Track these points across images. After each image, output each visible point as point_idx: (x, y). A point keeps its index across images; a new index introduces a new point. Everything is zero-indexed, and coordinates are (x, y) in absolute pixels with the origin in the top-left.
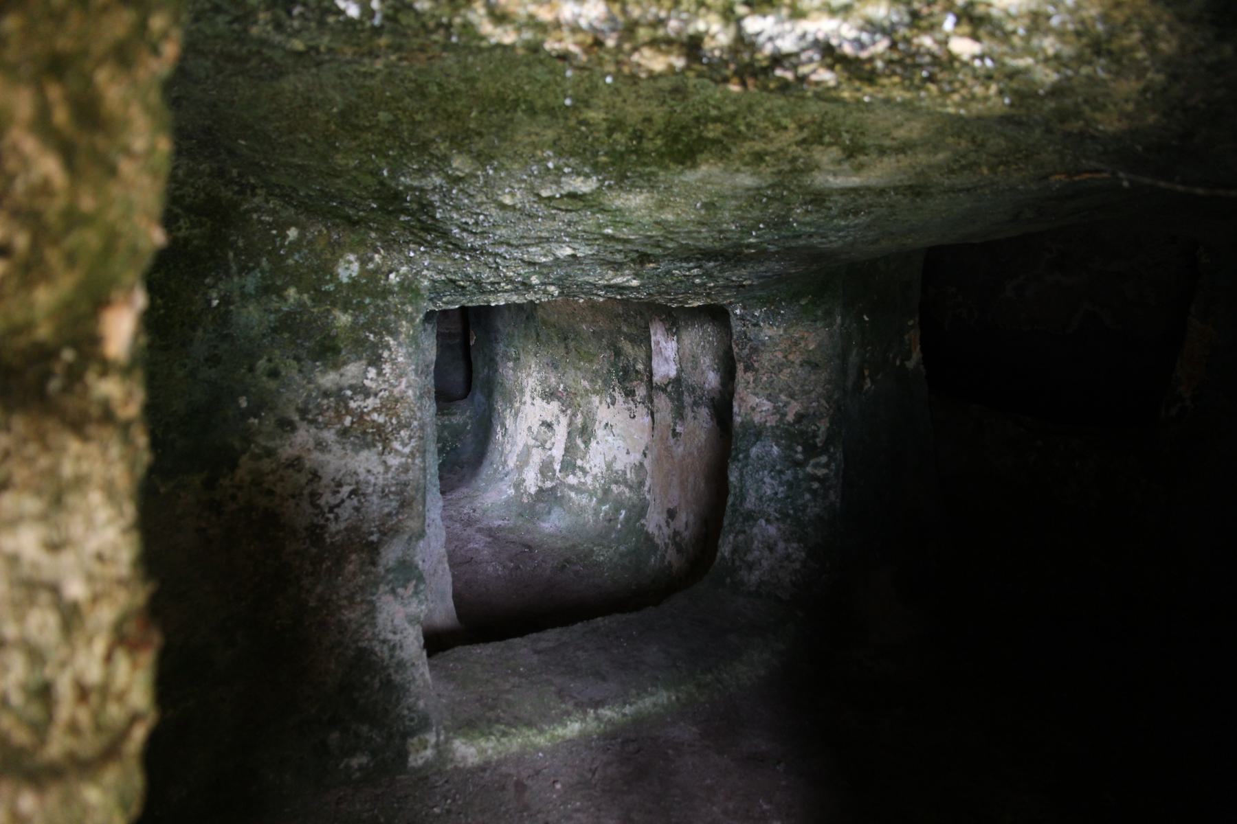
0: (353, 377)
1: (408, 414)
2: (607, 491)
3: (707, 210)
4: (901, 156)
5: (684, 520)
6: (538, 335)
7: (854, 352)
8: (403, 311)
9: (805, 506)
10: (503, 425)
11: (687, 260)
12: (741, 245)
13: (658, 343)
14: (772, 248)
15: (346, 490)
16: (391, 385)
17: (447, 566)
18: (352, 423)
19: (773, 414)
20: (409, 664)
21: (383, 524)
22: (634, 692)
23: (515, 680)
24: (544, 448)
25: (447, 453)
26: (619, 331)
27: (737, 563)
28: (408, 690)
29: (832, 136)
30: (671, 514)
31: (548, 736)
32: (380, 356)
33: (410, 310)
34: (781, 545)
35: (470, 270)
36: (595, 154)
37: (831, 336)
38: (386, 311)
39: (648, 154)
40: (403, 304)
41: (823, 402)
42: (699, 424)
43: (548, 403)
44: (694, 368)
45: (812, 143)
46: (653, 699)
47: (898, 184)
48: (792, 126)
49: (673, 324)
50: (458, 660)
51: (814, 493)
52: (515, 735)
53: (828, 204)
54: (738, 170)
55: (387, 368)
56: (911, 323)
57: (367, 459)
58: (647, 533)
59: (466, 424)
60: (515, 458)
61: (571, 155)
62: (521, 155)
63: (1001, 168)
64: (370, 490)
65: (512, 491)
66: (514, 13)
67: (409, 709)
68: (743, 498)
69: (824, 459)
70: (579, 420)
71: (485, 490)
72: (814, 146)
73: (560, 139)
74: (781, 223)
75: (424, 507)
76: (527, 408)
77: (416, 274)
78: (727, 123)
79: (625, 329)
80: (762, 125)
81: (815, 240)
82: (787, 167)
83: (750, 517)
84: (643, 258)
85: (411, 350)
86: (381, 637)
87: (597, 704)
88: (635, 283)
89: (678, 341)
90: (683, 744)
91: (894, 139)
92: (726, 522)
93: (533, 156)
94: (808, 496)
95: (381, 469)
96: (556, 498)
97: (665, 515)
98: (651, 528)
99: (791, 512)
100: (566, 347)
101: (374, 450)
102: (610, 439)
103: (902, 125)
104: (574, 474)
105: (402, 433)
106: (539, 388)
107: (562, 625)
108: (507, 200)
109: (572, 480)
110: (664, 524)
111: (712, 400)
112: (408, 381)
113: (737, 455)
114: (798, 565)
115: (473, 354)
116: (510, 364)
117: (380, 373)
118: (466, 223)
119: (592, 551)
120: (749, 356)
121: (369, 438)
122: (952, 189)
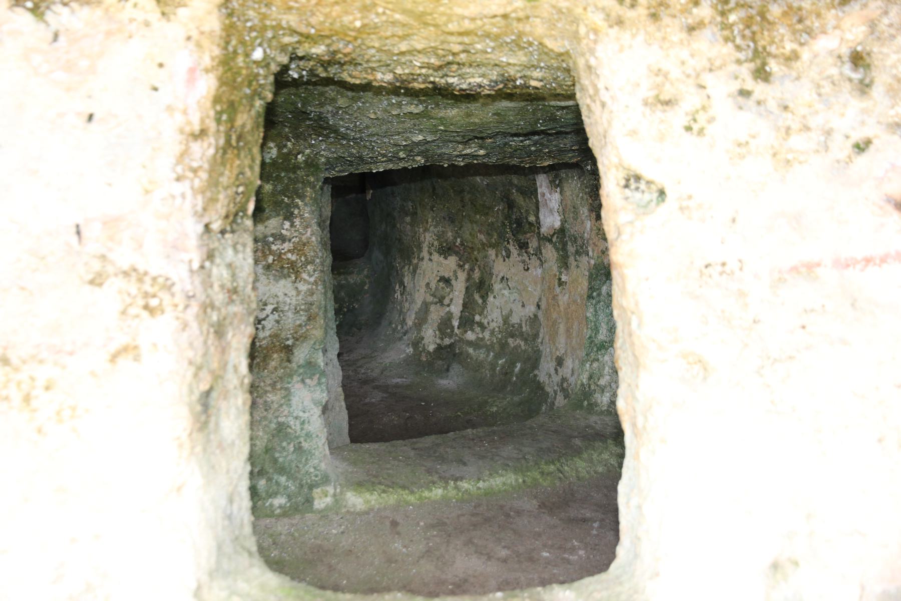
0: (274, 228)
1: (312, 254)
2: (503, 345)
5: (571, 367)
6: (434, 189)
8: (308, 181)
10: (402, 284)
13: (543, 195)
15: (269, 308)
16: (300, 233)
17: (343, 404)
18: (274, 260)
21: (296, 333)
24: (442, 305)
26: (511, 184)
27: (593, 387)
31: (417, 496)
32: (292, 213)
33: (312, 180)
35: (354, 151)
38: (295, 181)
40: (308, 176)
43: (446, 258)
44: (575, 219)
46: (503, 479)
52: (392, 493)
55: (297, 222)
57: (284, 286)
58: (539, 382)
60: (413, 316)
64: (286, 308)
65: (410, 350)
66: (324, 245)
70: (477, 275)
71: (384, 350)
76: (425, 265)
77: (316, 154)
79: (515, 181)
85: (313, 208)
86: (295, 415)
88: (482, 152)
89: (561, 193)
95: (294, 293)
96: (455, 355)
100: (462, 201)
101: (289, 279)
102: (506, 292)
104: (473, 330)
105: (309, 267)
106: (436, 243)
109: (470, 336)
110: (552, 371)
112: (312, 231)
116: (408, 219)
117: (292, 225)
121: (286, 271)
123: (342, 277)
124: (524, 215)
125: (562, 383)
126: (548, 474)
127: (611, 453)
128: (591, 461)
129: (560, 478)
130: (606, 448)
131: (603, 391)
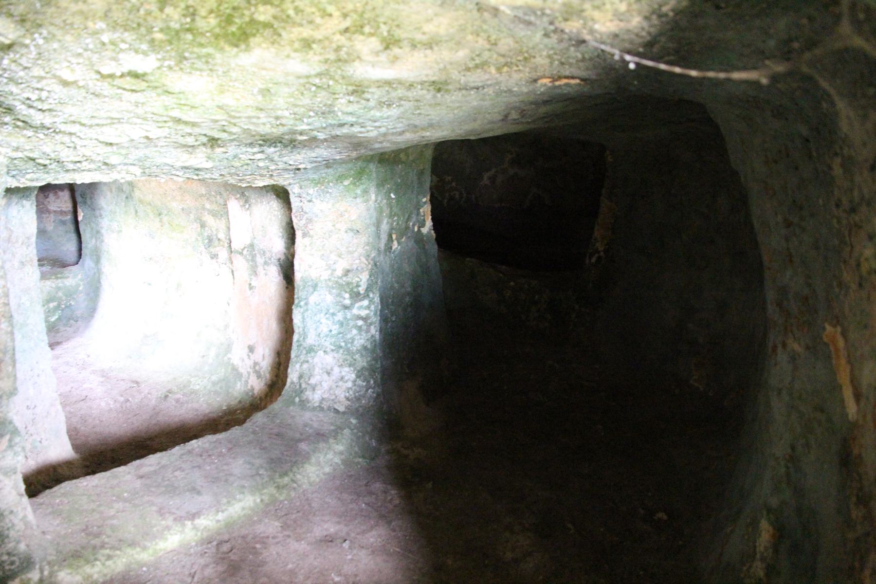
3: (264, 96)
4: (428, 52)
5: (262, 353)
6: (136, 212)
7: (385, 221)
9: (353, 339)
11: (251, 145)
12: (294, 132)
14: (321, 136)
19: (326, 270)
20: (6, 513)
22: (225, 500)
23: (119, 505)
25: (63, 310)
26: (204, 208)
27: (303, 386)
28: (8, 537)
29: (372, 27)
30: (251, 349)
34: (336, 370)
36: (150, 30)
37: (368, 210)
39: (202, 34)
41: (364, 260)
42: (273, 278)
45: (354, 33)
46: (241, 504)
47: (425, 79)
48: (336, 14)
49: (246, 201)
50: (64, 495)
51: (360, 328)
52: (119, 556)
53: (366, 96)
54: (288, 56)
56: (424, 200)
58: (233, 364)
59: (78, 286)
61: (126, 30)
62: (72, 24)
63: (505, 69)
67: (9, 554)
68: (305, 336)
69: (366, 303)
72: (356, 36)
73: (109, 10)
74: (327, 111)
75: (14, 366)
78: (277, 6)
79: (208, 206)
80: (309, 10)
81: (356, 129)
82: (332, 56)
83: (311, 350)
84: (213, 142)
87: (193, 516)
90: (268, 537)
91: (424, 33)
92: (293, 354)
93: (86, 28)
94: (355, 332)
97: (247, 350)
98: (236, 361)
99: (343, 344)
100: (161, 221)
103: (432, 20)
107: (161, 451)
108: (67, 76)
110: (246, 357)
111: (279, 260)
113: (299, 302)
114: (350, 384)
115: (80, 225)
118: (28, 99)
119: (190, 382)
120: (306, 226)
122: (466, 88)
123: (59, 281)
124: (215, 232)
125: (254, 367)
126: (283, 487)
127: (335, 453)
128: (319, 464)
129: (294, 488)
130: (329, 448)
131: (314, 389)
